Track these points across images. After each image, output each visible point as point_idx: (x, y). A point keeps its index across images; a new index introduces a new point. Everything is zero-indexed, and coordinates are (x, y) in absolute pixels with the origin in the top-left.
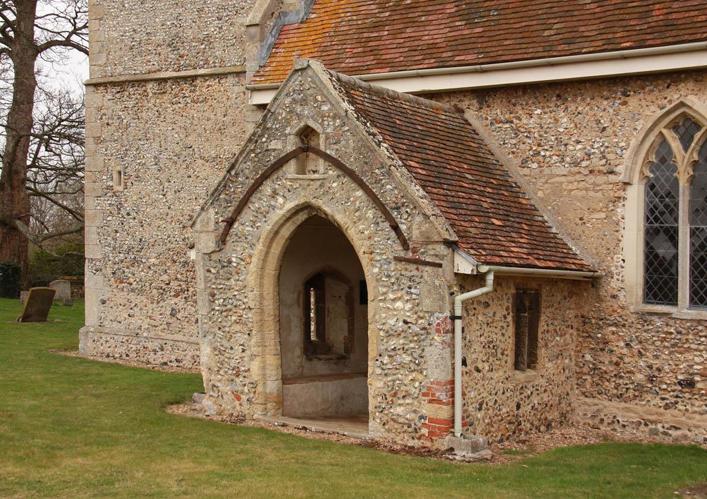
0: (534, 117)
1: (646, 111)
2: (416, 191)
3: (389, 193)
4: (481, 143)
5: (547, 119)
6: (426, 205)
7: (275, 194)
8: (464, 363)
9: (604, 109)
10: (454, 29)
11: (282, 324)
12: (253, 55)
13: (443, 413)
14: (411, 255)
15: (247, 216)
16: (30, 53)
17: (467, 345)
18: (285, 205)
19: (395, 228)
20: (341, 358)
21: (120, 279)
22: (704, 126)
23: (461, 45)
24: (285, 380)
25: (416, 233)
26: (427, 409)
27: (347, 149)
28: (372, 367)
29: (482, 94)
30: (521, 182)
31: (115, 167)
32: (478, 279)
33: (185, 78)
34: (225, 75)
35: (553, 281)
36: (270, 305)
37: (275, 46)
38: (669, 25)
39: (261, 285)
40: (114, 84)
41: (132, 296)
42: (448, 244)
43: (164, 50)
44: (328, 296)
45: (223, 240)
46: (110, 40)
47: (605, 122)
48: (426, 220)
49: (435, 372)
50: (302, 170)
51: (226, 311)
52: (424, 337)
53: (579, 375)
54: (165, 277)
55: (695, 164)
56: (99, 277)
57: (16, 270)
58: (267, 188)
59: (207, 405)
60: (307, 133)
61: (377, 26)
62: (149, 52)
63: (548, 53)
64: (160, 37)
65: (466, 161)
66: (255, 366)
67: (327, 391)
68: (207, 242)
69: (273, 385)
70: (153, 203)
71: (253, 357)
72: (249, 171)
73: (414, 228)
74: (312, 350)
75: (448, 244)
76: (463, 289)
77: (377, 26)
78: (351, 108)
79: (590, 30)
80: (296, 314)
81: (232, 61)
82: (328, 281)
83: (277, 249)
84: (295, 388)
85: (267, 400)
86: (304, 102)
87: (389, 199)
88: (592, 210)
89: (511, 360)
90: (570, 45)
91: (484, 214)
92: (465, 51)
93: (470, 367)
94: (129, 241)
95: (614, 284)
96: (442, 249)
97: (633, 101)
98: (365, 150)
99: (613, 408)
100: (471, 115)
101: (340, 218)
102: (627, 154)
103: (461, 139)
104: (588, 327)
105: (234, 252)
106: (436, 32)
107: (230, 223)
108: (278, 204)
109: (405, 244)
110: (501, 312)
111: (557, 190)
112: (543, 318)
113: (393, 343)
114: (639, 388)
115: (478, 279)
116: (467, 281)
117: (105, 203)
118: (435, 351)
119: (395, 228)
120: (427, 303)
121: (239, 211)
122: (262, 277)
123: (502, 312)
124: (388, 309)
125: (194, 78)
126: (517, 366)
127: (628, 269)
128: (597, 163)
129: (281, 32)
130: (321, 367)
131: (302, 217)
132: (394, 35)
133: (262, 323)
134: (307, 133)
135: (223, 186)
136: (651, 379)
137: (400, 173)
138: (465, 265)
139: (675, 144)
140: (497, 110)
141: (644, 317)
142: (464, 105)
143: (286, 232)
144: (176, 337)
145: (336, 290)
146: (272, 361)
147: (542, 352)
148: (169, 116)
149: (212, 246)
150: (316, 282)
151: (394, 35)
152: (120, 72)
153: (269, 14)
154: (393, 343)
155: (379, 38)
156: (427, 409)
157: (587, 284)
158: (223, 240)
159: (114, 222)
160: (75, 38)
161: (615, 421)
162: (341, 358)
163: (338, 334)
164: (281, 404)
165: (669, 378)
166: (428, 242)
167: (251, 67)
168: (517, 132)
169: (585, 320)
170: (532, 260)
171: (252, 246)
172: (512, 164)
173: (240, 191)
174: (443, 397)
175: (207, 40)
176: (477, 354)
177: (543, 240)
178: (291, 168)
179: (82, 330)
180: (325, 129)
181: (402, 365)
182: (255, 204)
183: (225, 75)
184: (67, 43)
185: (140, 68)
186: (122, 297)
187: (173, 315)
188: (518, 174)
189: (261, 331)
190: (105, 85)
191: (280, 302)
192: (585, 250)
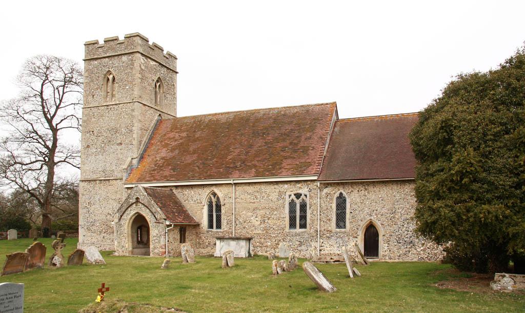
0: (187, 191)
1: (207, 191)
2: (159, 209)
3: (153, 210)
4: (176, 197)
5: (189, 192)
6: (161, 212)
7: (131, 210)
8: (168, 241)
9: (200, 190)
10: (171, 172)
11: (132, 237)
12: (125, 176)
13: (164, 250)
14: (158, 222)
15: (125, 215)
16: (52, 165)
17: (169, 238)
18: (133, 213)
19: (155, 216)
20: (146, 244)
21: (89, 229)
22: (7, 256)
23: (171, 176)
24: (133, 248)
25: (159, 217)
26: (161, 250)
27: (145, 202)
28: (151, 243)
29: (177, 187)
30: (184, 205)
31: (88, 201)
32: (171, 225)
33: (107, 180)
34: (117, 179)
35: (189, 225)
36: (130, 232)
37: (130, 173)
38: (210, 175)
39: (128, 228)
40: (88, 181)
41: (92, 234)
42: (165, 219)
43: (101, 173)
44: (143, 231)
45: (120, 220)
46: (87, 170)
47: (200, 193)
48: (160, 214)
49: (162, 243)
50: (136, 205)
51: (120, 234)
52: (160, 235)
53: (196, 244)
54: (101, 229)
55: (216, 202)
56: (83, 230)
57: (48, 229)
58: (129, 209)
59: (116, 254)
60: (137, 198)
61: (154, 170)
62: (97, 173)
63: (189, 179)
64: (100, 169)
65: (171, 201)
66: (127, 245)
67: (143, 250)
68: (116, 220)
69: (130, 249)
70: (98, 210)
71: (126, 243)
72: (125, 206)
73: (158, 216)
74: (139, 242)
75: (165, 219)
76: (168, 227)
77: (154, 170)
78: (146, 194)
79: (196, 175)
80: (136, 234)
81: (119, 176)
82: (143, 228)
83: (131, 221)
84: (135, 250)
85: (129, 251)
86: (137, 193)
87: (153, 211)
88: (198, 211)
89: (179, 241)
90: (193, 178)
91: (173, 213)
92: (172, 178)
93: (169, 242)
94: (91, 220)
95: (202, 225)
96: (163, 220)
97: (205, 189)
98: (148, 202)
99: (202, 250)
100: (174, 191)
101: (144, 215)
102: (204, 199)
103: (172, 197)
104: (197, 234)
105: (122, 222)
106: (167, 173)
107: (121, 216)
108: (132, 212)
109: (157, 220)
110: (176, 232)
111: (191, 207)
112: (187, 233)
113: (155, 238)
114: (207, 246)
115: (171, 225)
116: (168, 226)
117: (85, 211)
118: (162, 239)
119: (155, 216)
120: (161, 230)
121: (123, 214)
122: (128, 227)
123: (177, 232)
124: (153, 232)
125: (109, 180)
126: (181, 242)
127: (205, 222)
128: (199, 201)
129: (132, 170)
130: (141, 246)
131: (137, 215)
132: (158, 172)
133: (128, 236)
134: (137, 198)
135: (120, 209)
136: (209, 244)
137: (156, 206)
138: (168, 223)
139: (213, 198)
140: (180, 190)
141: (208, 232)
142: (173, 188)
143: (133, 218)
144: (105, 243)
145: (144, 229)
146: (130, 244)
147: (187, 240)
148: (103, 189)
149: (117, 221)
150: (140, 228)
151: (158, 172)
152: (89, 178)
153: (129, 166)
154: (155, 238)
155: (155, 173)
156: (161, 250)
157: (197, 226)
158: (120, 220)
159: (87, 215)
160: (67, 160)
161: (202, 253)
162: (146, 244)
163: (145, 239)
164: (132, 253)
165: (212, 243)
166: (161, 219)
167: (124, 178)
168: (183, 194)
169: (197, 233)
170: (183, 221)
171: (126, 221)
172: (182, 201)
173: (123, 210)
174: (164, 247)
175: (113, 171)
176: (171, 240)
177: (188, 217)
178: (134, 205)
179: (78, 243)
180: (141, 198)
181: (156, 242)
182: (127, 212)
183: (117, 179)
184: (64, 161)
185: (94, 177)
186: (89, 234)
187: (103, 238)
188: (184, 203)
189: (128, 238)
190: (85, 181)
191: (132, 232)
192: (196, 219)
